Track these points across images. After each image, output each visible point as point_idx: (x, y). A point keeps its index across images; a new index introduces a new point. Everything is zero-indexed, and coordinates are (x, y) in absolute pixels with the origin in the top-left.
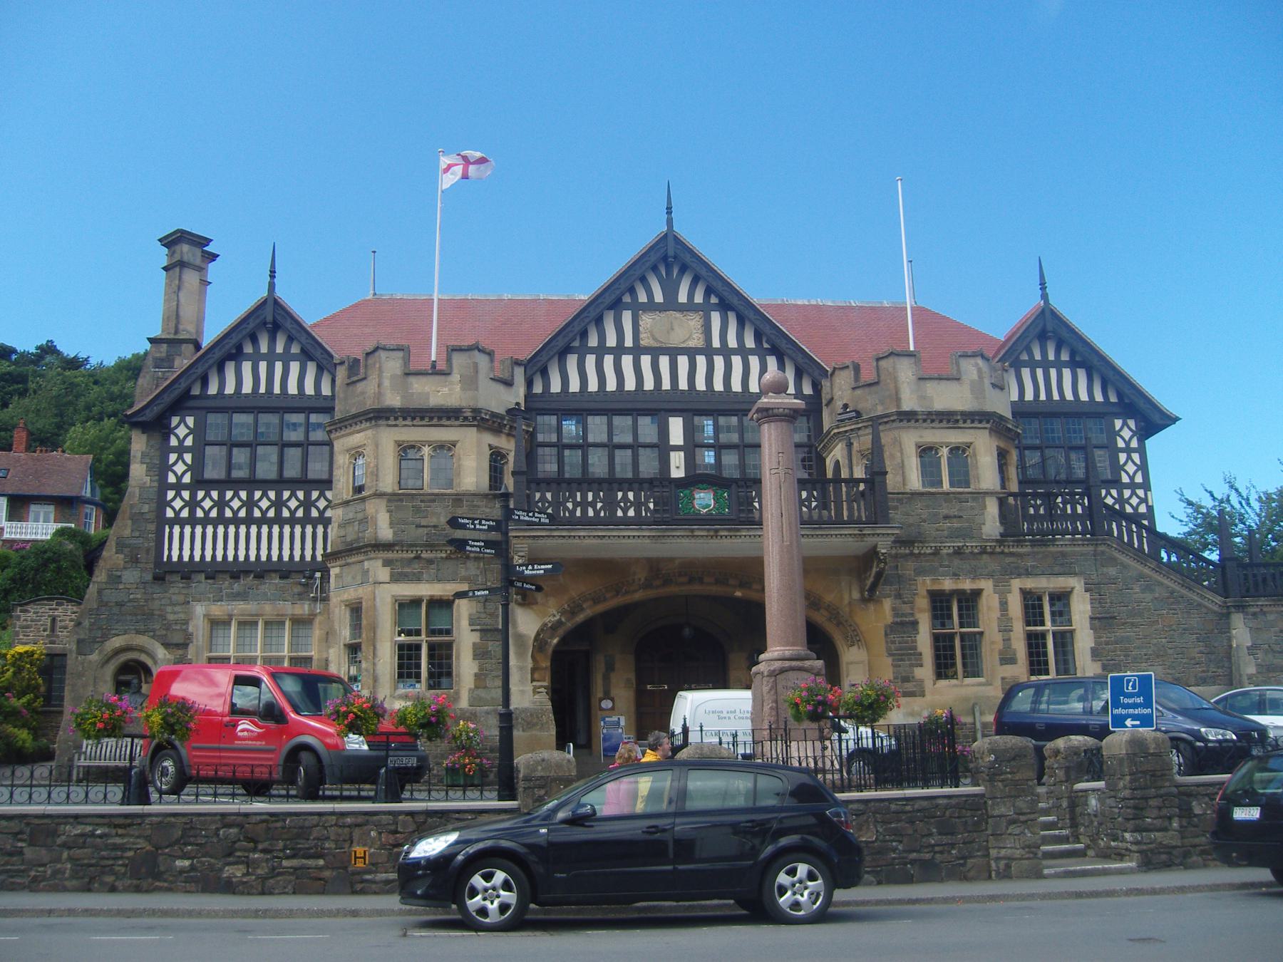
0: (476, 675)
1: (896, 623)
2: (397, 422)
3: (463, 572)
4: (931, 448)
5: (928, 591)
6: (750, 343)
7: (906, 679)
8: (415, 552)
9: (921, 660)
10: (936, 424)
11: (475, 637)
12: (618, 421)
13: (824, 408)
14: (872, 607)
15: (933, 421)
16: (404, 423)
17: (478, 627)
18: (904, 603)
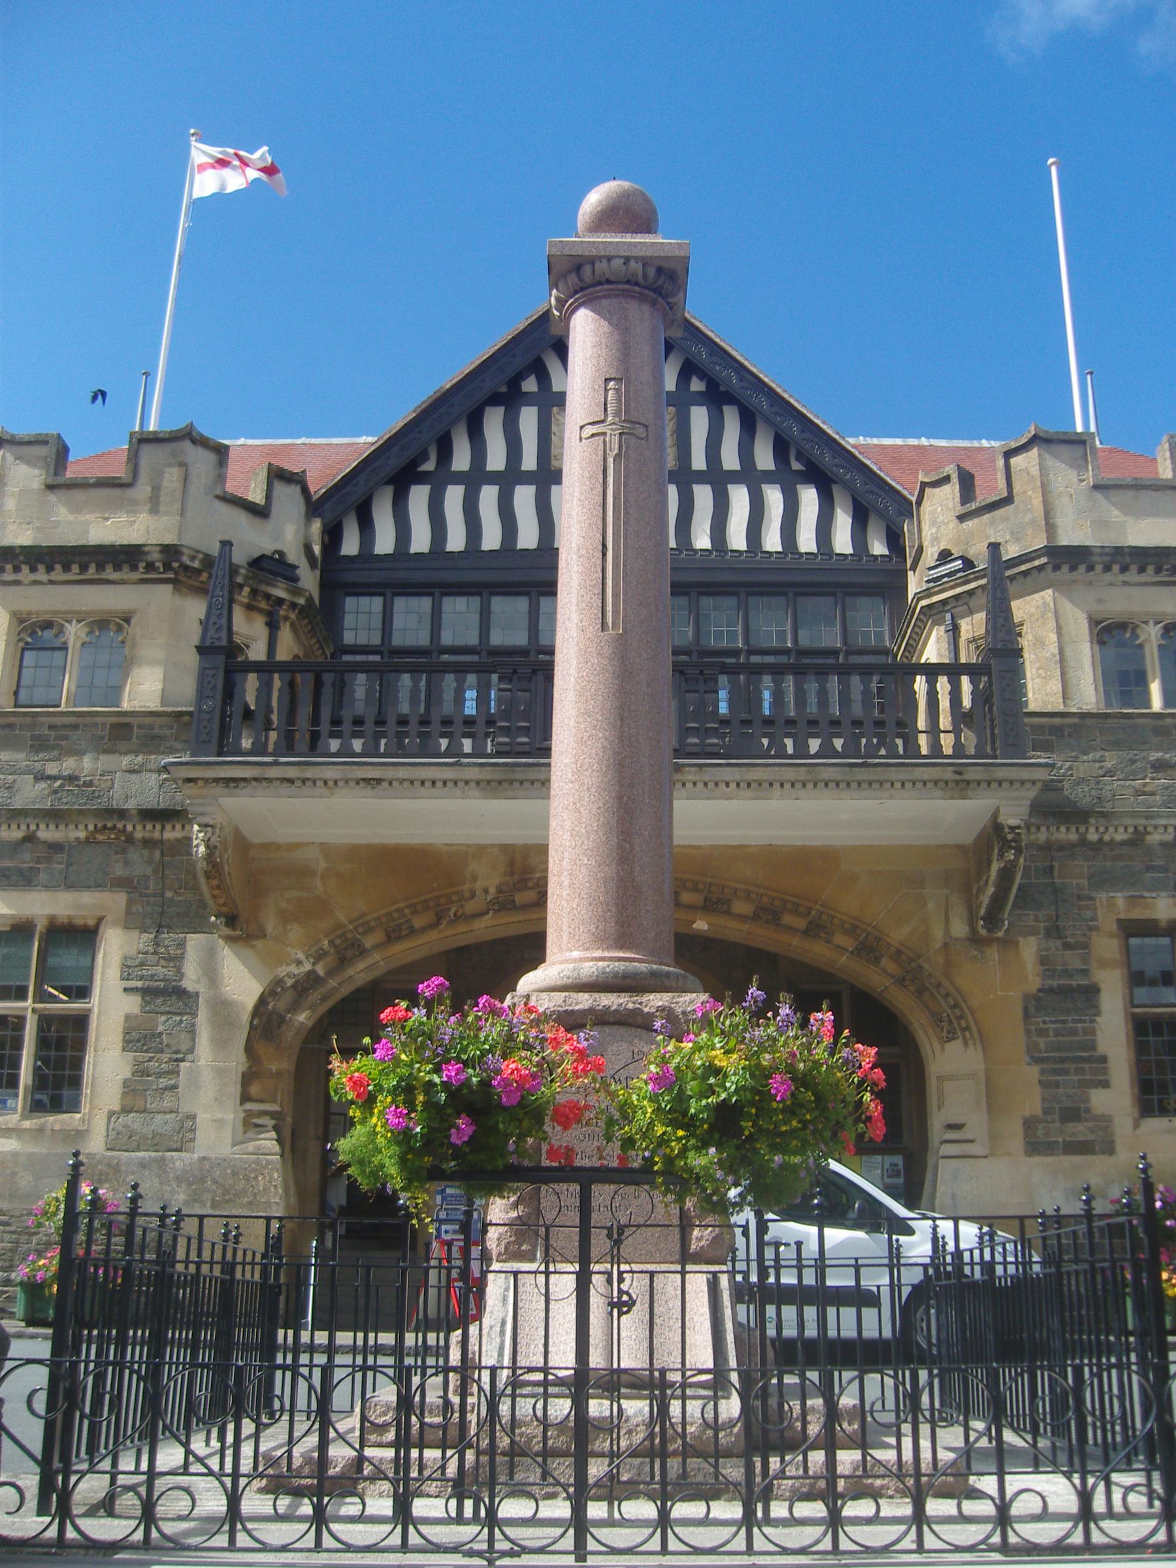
0: (126, 1083)
1: (1050, 990)
2: (18, 577)
3: (119, 871)
4: (1122, 626)
5: (1119, 921)
6: (765, 459)
7: (1072, 1114)
8: (24, 827)
9: (1105, 1071)
10: (1132, 576)
11: (132, 1004)
12: (499, 604)
13: (910, 573)
14: (993, 954)
15: (1124, 569)
16: (33, 577)
17: (139, 984)
18: (1067, 946)
